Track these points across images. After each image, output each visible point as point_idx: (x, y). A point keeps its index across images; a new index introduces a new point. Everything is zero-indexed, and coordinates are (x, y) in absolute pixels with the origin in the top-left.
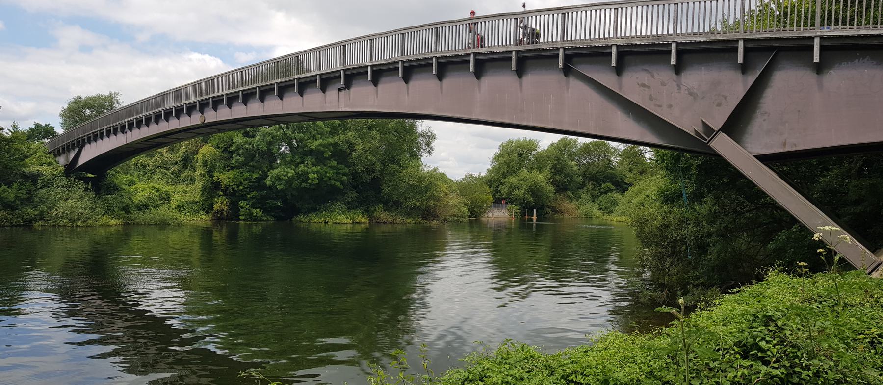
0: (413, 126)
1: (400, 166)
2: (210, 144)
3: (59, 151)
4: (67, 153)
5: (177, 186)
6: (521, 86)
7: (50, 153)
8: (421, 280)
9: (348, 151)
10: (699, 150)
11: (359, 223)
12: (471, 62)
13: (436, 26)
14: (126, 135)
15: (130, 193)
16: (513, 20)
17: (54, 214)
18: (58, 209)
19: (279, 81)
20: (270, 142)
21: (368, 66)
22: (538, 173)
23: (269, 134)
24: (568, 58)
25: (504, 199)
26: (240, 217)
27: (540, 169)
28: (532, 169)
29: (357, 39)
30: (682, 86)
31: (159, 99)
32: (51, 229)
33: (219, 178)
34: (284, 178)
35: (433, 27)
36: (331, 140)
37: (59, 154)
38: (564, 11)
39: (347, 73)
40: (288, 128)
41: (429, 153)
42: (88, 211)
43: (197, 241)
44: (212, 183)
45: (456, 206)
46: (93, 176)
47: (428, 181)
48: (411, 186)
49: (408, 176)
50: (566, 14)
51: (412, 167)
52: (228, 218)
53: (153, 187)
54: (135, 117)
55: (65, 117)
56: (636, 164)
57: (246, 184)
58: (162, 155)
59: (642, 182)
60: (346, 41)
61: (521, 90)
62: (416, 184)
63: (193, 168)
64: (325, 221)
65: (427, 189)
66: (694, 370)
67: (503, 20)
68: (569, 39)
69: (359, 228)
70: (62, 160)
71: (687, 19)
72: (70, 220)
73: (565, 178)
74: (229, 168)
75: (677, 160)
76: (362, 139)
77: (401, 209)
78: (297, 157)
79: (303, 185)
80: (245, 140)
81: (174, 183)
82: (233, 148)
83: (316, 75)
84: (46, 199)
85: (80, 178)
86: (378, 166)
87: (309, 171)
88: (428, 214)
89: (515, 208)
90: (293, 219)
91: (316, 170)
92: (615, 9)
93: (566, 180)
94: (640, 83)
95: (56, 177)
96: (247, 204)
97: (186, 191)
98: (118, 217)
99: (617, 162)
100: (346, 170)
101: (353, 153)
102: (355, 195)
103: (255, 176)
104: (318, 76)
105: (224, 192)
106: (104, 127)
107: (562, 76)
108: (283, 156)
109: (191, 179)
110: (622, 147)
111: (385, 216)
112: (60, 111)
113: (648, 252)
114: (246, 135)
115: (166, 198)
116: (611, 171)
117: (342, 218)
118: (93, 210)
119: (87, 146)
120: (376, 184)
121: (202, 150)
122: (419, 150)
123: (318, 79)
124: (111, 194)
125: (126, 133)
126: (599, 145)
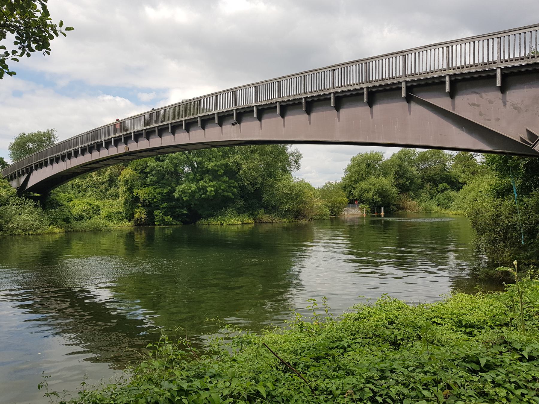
0: (284, 149)
1: (276, 179)
2: (130, 167)
3: (11, 176)
4: (18, 179)
5: (105, 201)
6: (372, 113)
7: (4, 178)
8: (295, 268)
9: (237, 169)
10: (525, 153)
11: (247, 224)
12: (332, 99)
13: (304, 75)
14: (65, 162)
15: (69, 207)
16: (364, 64)
17: (11, 226)
18: (14, 222)
19: (186, 118)
20: (176, 164)
21: (254, 106)
22: (384, 178)
23: (175, 158)
24: (409, 89)
25: (357, 200)
26: (156, 223)
27: (385, 175)
28: (379, 175)
29: (244, 86)
30: (507, 103)
31: (91, 134)
32: (9, 238)
33: (138, 194)
34: (188, 191)
35: (301, 75)
36: (224, 162)
37: (12, 179)
38: (404, 54)
39: (238, 112)
40: (190, 153)
41: (298, 168)
42: (37, 223)
43: (122, 241)
44: (133, 197)
45: (320, 208)
46: (39, 195)
47: (297, 189)
48: (285, 194)
49: (282, 187)
50: (406, 55)
51: (285, 180)
52: (146, 224)
53: (87, 202)
54: (73, 149)
55: (13, 150)
56: (468, 167)
57: (159, 197)
58: (92, 177)
59: (474, 181)
60: (236, 88)
61: (372, 117)
62: (289, 192)
63: (117, 186)
64: (221, 223)
65: (297, 196)
66: (527, 315)
67: (356, 65)
68: (409, 73)
69: (246, 227)
70: (14, 184)
71: (509, 49)
72: (23, 230)
73: (407, 181)
74: (145, 185)
75: (506, 161)
76: (247, 160)
77: (278, 212)
78: (197, 175)
79: (203, 196)
80: (157, 163)
81: (103, 198)
82: (148, 170)
83: (214, 114)
84: (4, 214)
85: (30, 197)
86: (260, 180)
87: (207, 185)
88: (298, 214)
89: (365, 207)
90: (197, 223)
91: (212, 185)
92: (446, 47)
93: (407, 183)
94: (470, 103)
95: (10, 197)
96: (160, 213)
97: (112, 204)
98: (61, 226)
99: (451, 166)
100: (236, 184)
101: (241, 171)
102: (243, 202)
103: (166, 191)
104: (216, 114)
105: (142, 204)
106: (48, 157)
107: (405, 103)
108: (187, 175)
109: (116, 195)
110: (455, 153)
111: (266, 218)
112: (9, 146)
113: (483, 239)
114: (158, 159)
115: (97, 210)
116: (446, 173)
117: (233, 221)
118: (41, 221)
119: (35, 172)
120: (258, 194)
121: (123, 173)
122: (289, 165)
123: (216, 116)
124: (54, 209)
125: (66, 161)
126: (434, 153)
